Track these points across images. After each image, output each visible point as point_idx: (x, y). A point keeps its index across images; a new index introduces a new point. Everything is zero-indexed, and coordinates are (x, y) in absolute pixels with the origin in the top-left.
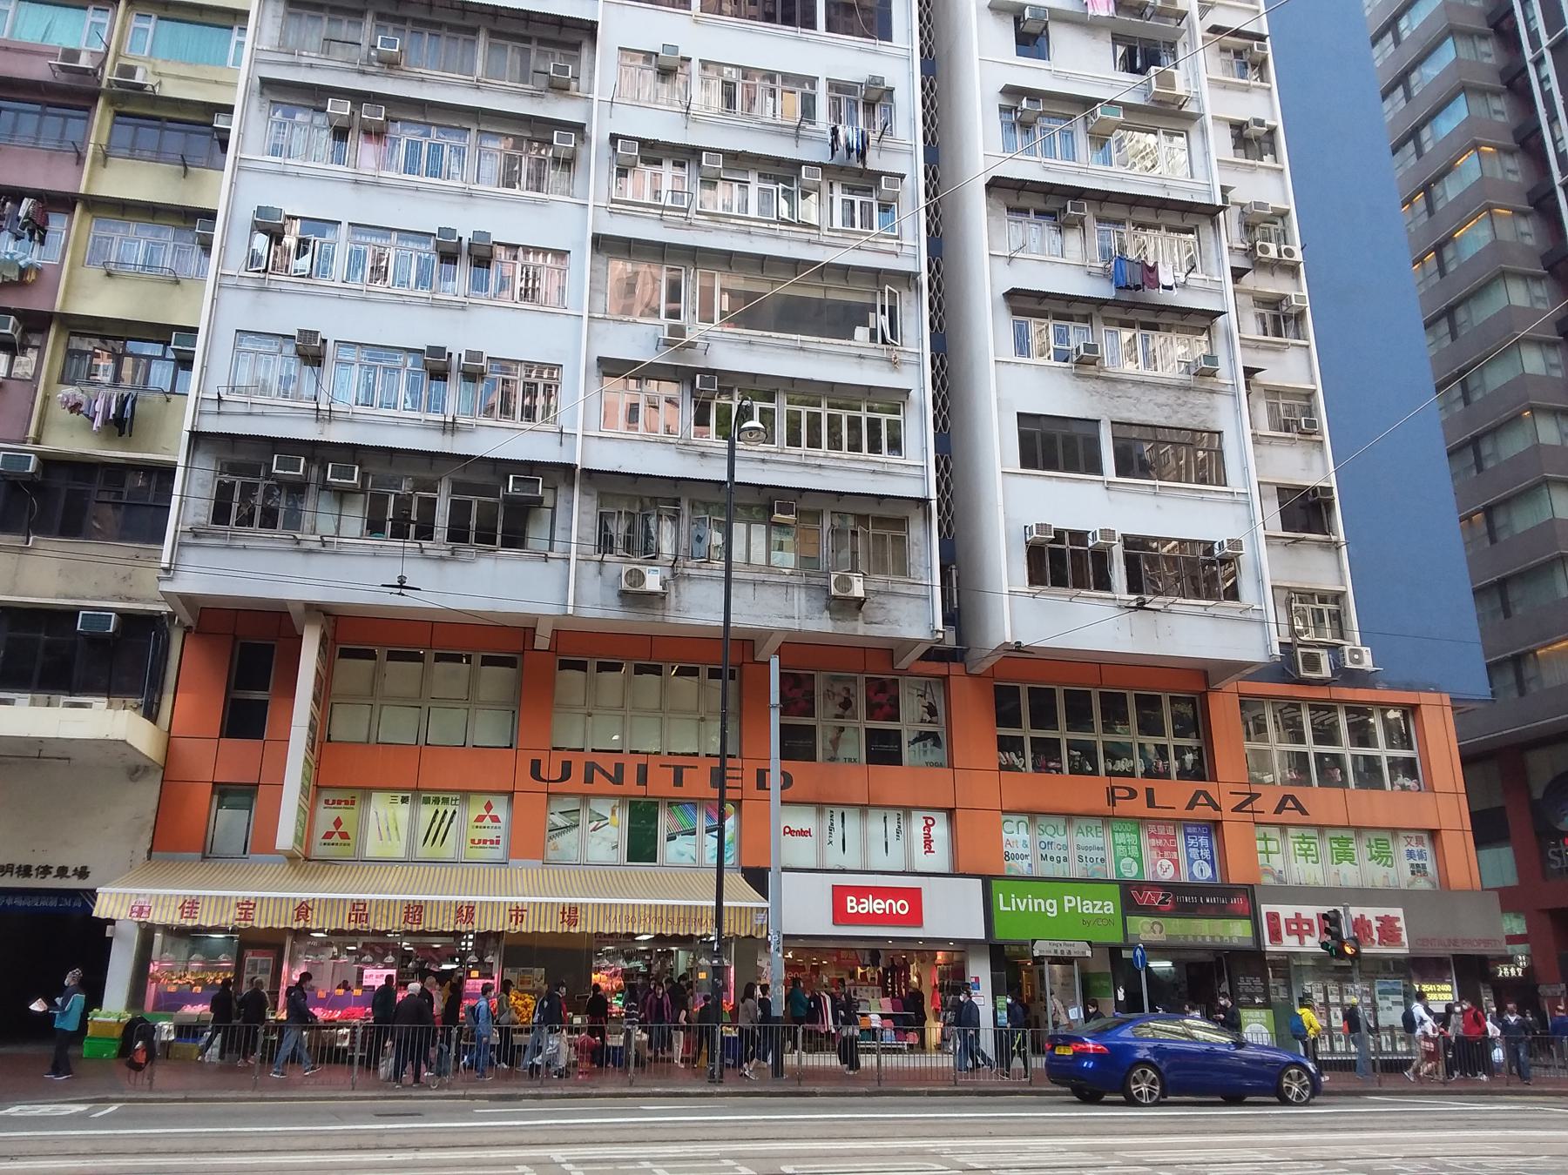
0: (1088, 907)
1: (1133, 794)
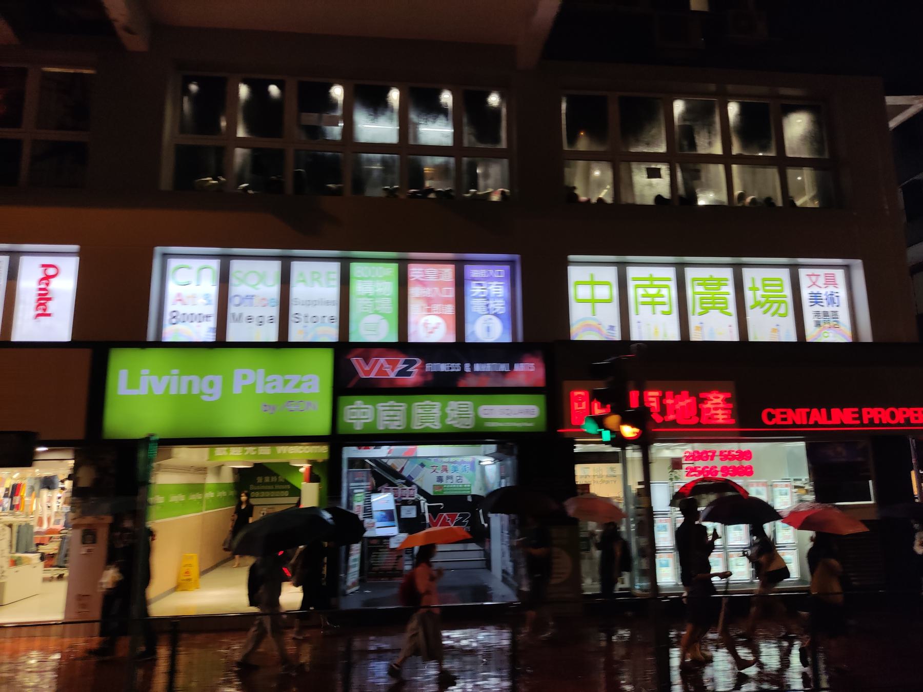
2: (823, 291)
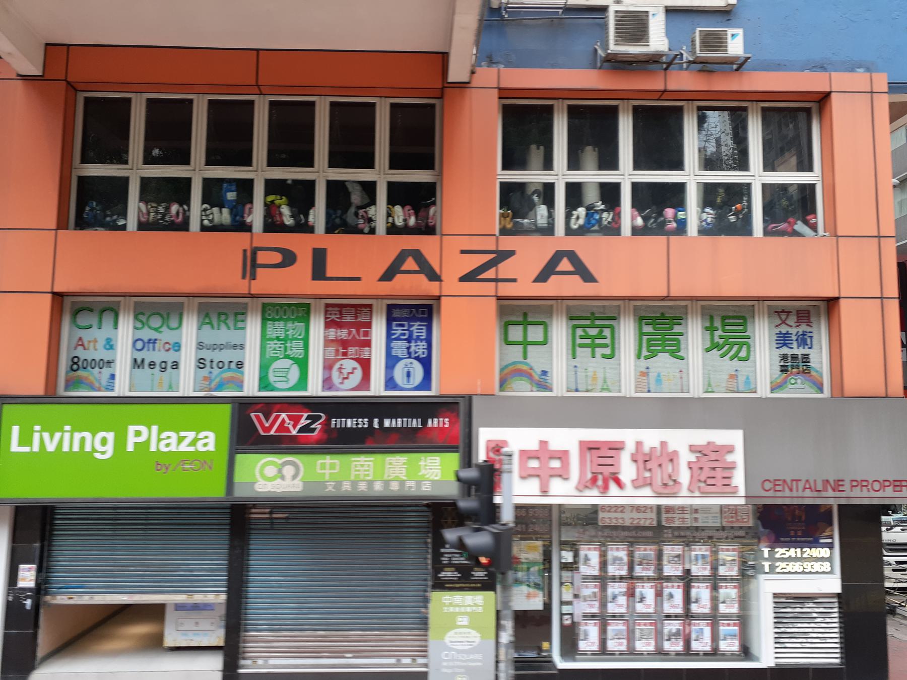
0: (170, 442)
1: (289, 259)
2: (793, 331)
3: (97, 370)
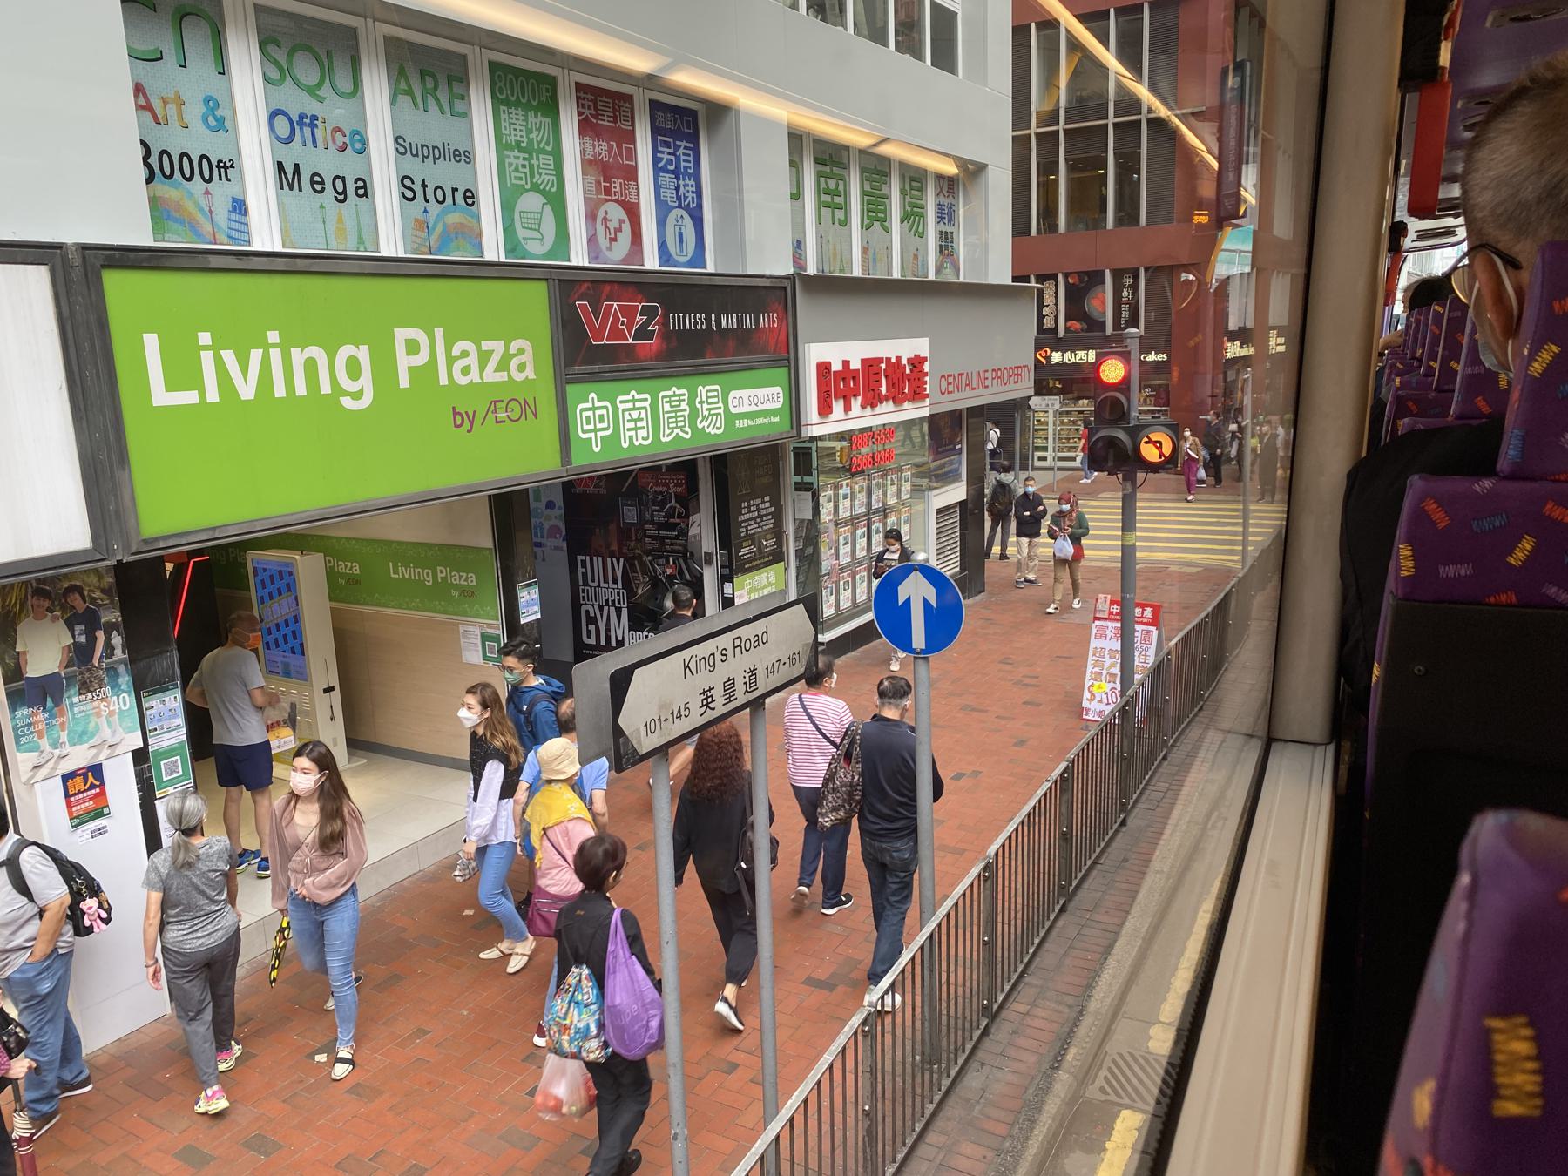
3: (198, 184)
